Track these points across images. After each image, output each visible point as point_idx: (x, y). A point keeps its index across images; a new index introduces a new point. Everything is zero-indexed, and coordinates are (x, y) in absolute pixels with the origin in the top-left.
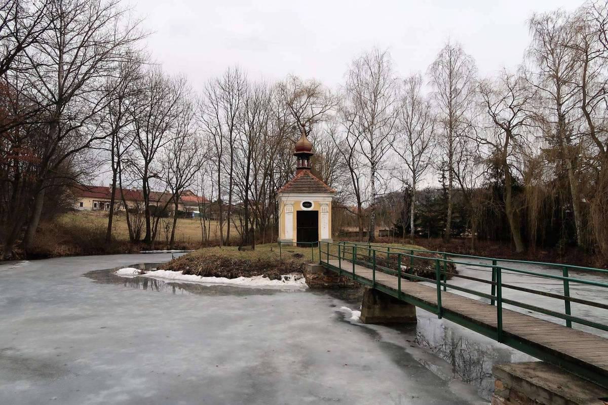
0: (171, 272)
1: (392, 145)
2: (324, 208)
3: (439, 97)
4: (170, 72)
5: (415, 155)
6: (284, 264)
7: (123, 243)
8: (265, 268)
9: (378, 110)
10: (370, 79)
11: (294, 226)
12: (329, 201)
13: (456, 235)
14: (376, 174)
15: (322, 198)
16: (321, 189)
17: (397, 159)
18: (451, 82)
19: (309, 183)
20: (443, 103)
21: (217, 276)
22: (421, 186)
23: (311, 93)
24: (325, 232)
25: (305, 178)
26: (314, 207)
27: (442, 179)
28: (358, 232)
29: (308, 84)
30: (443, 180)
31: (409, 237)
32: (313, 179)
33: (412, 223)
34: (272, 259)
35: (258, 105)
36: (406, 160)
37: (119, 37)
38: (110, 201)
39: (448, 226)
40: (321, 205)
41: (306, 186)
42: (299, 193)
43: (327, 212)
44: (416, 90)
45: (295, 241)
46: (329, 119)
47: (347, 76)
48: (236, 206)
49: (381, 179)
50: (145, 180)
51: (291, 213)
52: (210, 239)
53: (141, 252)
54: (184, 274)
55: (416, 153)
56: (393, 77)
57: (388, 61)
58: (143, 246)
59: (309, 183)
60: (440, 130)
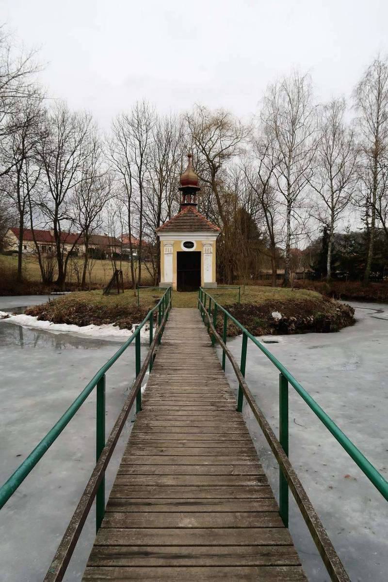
0: (30, 317)
1: (308, 181)
2: (207, 248)
3: (364, 123)
4: (75, 107)
5: (334, 190)
6: (140, 311)
7: (35, 284)
8: (120, 315)
10: (287, 107)
11: (174, 268)
12: (214, 241)
13: (378, 278)
14: (292, 213)
16: (204, 227)
17: (315, 196)
18: (379, 106)
19: (192, 220)
20: (367, 127)
21: (69, 323)
22: (340, 228)
23: (221, 124)
24: (208, 274)
25: (188, 215)
26: (197, 246)
27: (365, 217)
29: (215, 115)
31: (325, 280)
32: (197, 216)
33: (328, 264)
34: (130, 306)
35: (167, 142)
36: (323, 196)
37: (13, 70)
39: (368, 268)
40: (203, 245)
41: (188, 224)
42: (178, 231)
43: (211, 253)
44: (340, 116)
45: (175, 286)
46: (243, 152)
47: (262, 105)
48: (344, 253)
49: (299, 219)
50: (56, 221)
53: (52, 293)
54: (39, 319)
55: (335, 187)
57: (309, 85)
58: (55, 287)
59: (192, 220)
60: (364, 160)
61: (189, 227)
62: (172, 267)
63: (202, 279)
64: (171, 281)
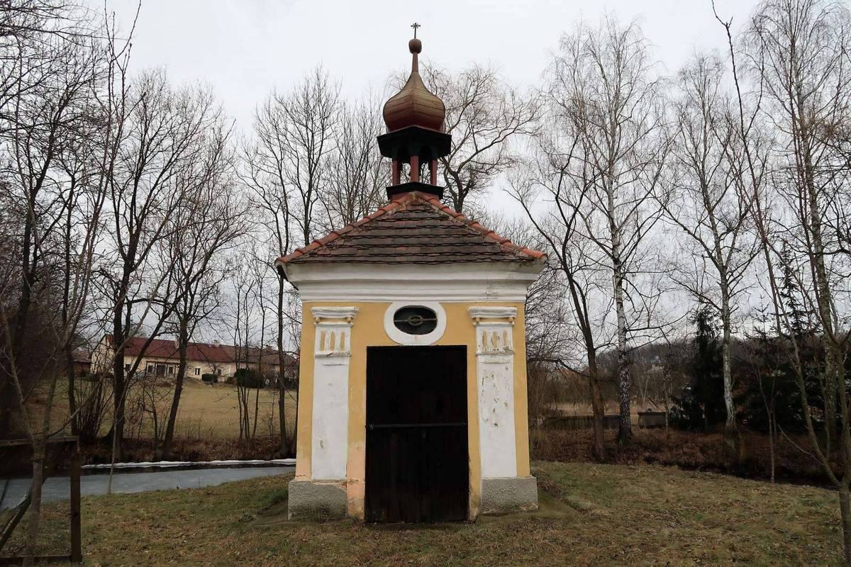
2: (490, 332)
9: (621, 147)
11: (352, 415)
12: (516, 303)
15: (483, 290)
19: (427, 231)
25: (413, 215)
28: (592, 418)
30: (789, 292)
38: (179, 362)
40: (475, 321)
45: (357, 493)
51: (340, 356)
52: (258, 433)
56: (651, 76)
59: (427, 231)
61: (416, 250)
62: (345, 409)
63: (472, 464)
64: (340, 473)
